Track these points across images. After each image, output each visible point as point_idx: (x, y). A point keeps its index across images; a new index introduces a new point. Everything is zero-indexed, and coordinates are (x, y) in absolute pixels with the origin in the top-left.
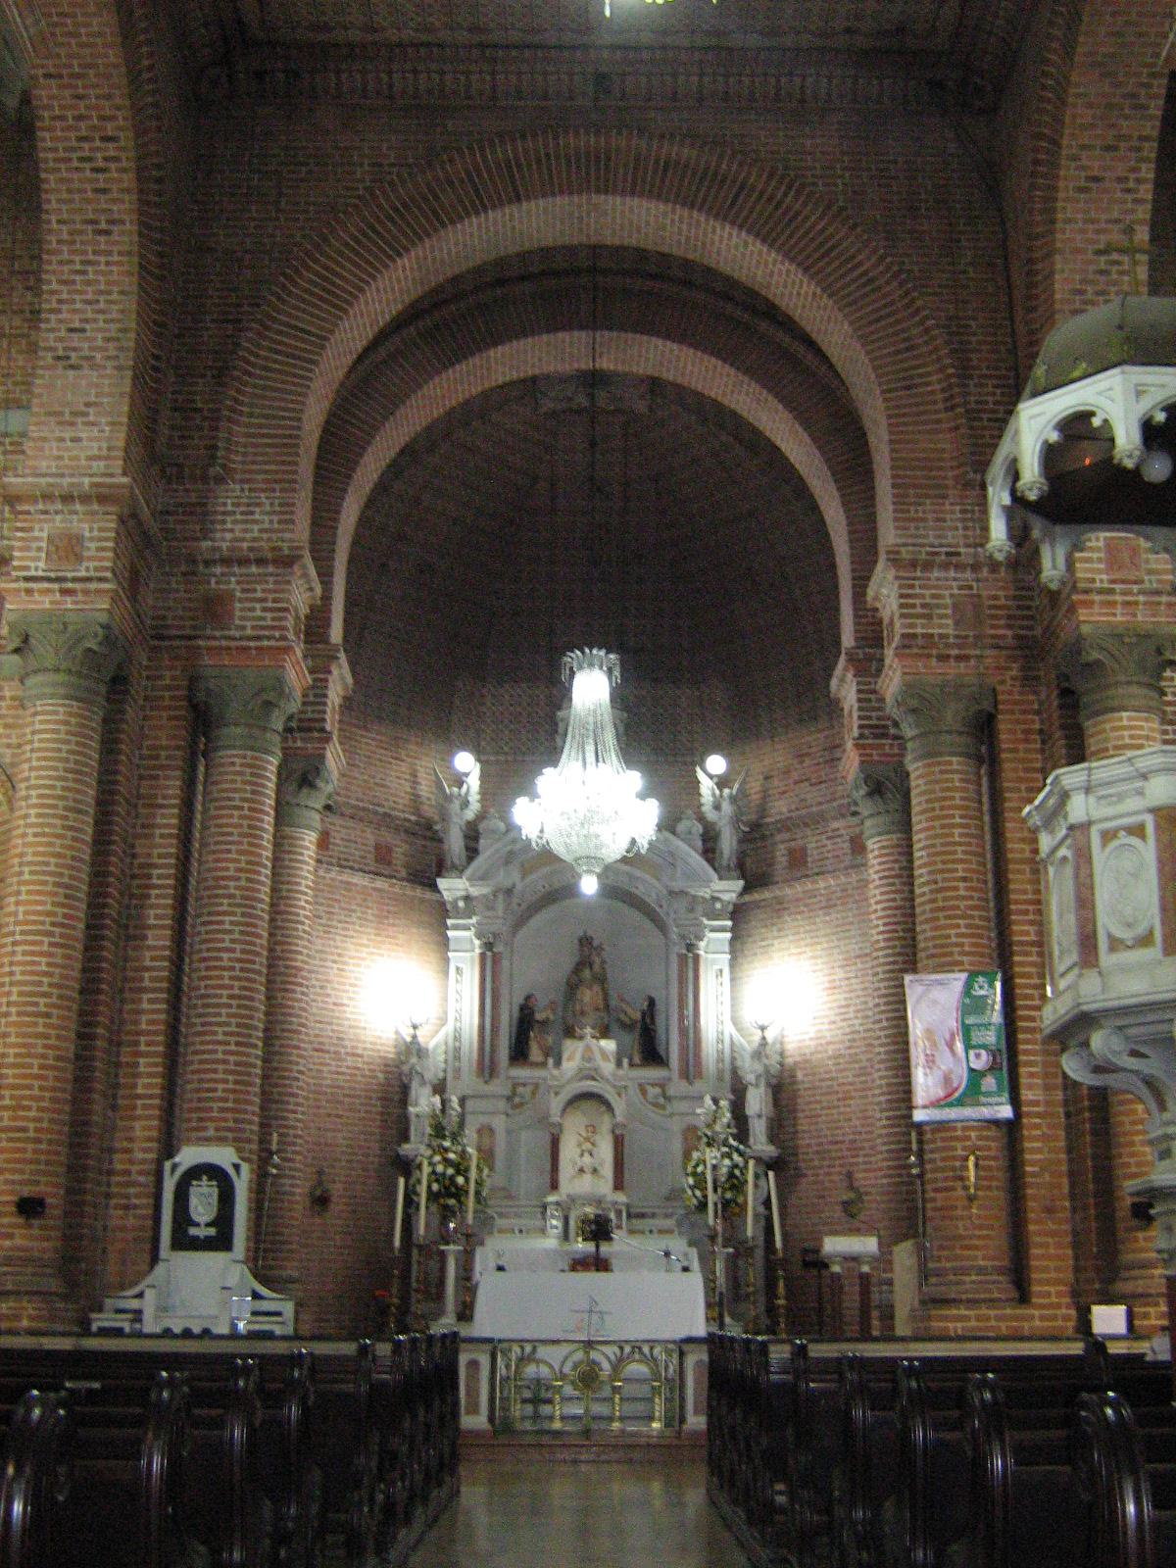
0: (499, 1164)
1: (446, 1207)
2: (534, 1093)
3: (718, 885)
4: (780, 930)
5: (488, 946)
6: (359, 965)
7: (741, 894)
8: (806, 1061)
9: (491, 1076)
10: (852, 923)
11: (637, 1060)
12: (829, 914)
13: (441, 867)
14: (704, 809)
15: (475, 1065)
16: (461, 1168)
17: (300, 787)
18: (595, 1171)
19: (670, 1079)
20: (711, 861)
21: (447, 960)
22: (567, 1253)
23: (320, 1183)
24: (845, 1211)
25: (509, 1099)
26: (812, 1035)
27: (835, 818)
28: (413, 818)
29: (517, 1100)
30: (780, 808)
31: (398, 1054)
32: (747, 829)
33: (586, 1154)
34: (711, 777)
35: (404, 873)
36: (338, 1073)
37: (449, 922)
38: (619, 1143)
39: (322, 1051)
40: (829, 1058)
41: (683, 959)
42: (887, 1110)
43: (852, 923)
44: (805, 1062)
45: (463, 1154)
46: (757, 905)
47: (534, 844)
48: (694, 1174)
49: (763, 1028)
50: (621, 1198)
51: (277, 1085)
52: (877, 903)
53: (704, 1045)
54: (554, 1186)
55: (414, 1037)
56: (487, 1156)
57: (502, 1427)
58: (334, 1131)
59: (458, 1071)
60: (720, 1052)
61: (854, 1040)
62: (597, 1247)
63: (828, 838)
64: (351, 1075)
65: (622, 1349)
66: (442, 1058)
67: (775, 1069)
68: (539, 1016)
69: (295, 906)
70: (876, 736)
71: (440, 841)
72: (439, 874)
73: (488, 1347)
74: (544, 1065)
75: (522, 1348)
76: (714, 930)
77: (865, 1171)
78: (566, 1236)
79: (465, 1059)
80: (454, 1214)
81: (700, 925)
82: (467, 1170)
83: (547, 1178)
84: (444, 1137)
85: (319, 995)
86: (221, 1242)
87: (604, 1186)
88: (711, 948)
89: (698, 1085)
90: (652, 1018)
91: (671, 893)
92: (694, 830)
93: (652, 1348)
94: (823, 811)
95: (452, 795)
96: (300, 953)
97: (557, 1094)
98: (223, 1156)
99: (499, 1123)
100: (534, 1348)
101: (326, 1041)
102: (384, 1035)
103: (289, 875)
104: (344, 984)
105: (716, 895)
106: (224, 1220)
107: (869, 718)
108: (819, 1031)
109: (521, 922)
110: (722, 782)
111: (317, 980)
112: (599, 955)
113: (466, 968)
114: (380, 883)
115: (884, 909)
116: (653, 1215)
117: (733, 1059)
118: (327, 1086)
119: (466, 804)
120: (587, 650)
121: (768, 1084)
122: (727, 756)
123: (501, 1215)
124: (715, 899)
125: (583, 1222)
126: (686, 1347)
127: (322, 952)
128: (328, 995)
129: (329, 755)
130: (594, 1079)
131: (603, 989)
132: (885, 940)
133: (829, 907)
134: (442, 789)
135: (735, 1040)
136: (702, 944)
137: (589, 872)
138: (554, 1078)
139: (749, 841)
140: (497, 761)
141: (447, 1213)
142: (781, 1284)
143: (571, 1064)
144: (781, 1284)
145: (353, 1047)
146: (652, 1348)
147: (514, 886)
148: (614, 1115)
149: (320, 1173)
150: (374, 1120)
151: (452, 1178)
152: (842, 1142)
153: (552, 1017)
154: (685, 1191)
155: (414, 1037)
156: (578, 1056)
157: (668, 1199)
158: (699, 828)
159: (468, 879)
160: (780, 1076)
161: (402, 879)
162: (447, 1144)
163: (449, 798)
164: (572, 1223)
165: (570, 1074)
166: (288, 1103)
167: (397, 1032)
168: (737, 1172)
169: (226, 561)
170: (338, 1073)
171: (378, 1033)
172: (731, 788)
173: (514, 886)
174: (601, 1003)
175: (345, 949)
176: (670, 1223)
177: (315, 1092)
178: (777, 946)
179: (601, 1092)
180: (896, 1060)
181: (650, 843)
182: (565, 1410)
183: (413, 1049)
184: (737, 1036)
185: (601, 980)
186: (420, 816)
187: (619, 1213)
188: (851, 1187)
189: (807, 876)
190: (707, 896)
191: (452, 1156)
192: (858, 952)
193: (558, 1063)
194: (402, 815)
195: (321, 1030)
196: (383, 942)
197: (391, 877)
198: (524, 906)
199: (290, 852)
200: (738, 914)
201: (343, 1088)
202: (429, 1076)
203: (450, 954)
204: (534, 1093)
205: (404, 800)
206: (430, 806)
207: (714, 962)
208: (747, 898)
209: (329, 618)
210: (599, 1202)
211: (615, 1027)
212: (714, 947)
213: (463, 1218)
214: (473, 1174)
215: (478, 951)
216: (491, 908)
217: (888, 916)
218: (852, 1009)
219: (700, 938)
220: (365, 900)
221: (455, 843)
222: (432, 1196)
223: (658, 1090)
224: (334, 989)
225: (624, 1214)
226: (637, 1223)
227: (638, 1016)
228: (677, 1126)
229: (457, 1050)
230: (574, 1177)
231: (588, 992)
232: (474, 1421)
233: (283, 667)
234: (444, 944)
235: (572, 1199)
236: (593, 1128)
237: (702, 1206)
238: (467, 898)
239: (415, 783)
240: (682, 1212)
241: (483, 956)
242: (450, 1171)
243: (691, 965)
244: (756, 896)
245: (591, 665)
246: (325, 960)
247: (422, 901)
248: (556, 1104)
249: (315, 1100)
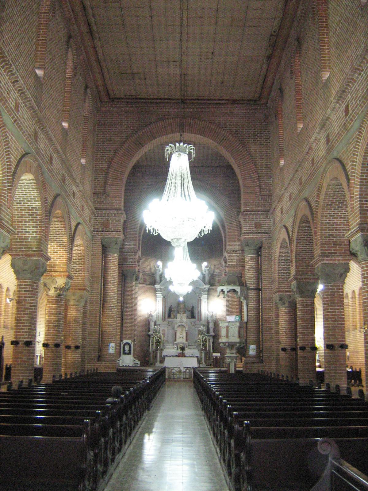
3: (205, 286)
5: (164, 297)
21: (156, 299)
30: (217, 271)
45: (160, 336)
50: (187, 343)
54: (175, 340)
57: (169, 378)
59: (158, 319)
67: (215, 319)
79: (160, 318)
86: (130, 353)
87: (184, 341)
90: (193, 310)
98: (130, 342)
99: (166, 329)
106: (130, 350)
110: (206, 267)
113: (160, 301)
114: (144, 285)
122: (208, 262)
143: (178, 320)
163: (157, 270)
169: (127, 252)
176: (195, 347)
182: (176, 376)
183: (150, 315)
184: (208, 313)
200: (209, 291)
205: (148, 269)
210: (183, 343)
212: (204, 297)
214: (162, 339)
221: (158, 279)
222: (156, 343)
226: (190, 347)
229: (158, 317)
232: (167, 377)
234: (156, 296)
235: (179, 343)
236: (182, 330)
238: (160, 288)
241: (163, 299)
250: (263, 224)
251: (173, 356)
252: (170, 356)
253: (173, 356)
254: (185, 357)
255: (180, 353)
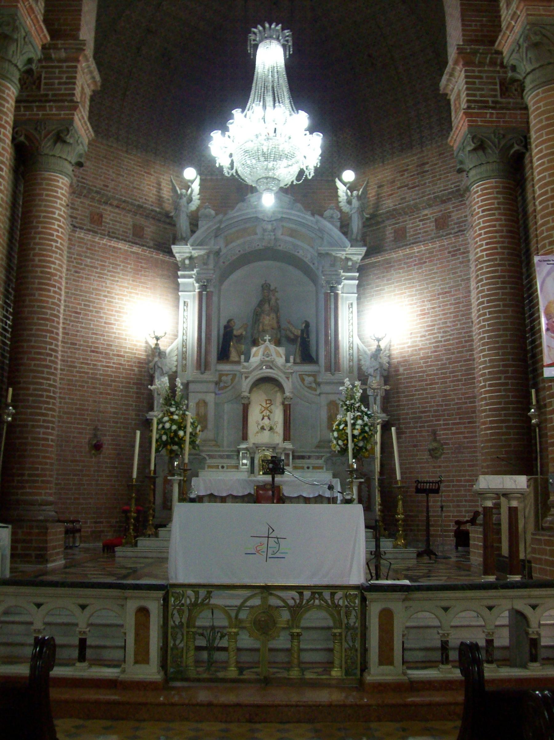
0: (211, 425)
1: (172, 451)
2: (233, 380)
4: (388, 280)
5: (203, 288)
6: (122, 300)
7: (363, 259)
8: (406, 361)
9: (205, 369)
10: (436, 273)
11: (298, 360)
12: (421, 268)
13: (175, 240)
14: (341, 204)
15: (195, 361)
16: (182, 426)
17: (55, 143)
18: (271, 429)
19: (319, 372)
20: (345, 234)
21: (178, 298)
22: (254, 481)
23: (95, 436)
24: (431, 455)
25: (217, 383)
26: (409, 344)
27: (424, 208)
28: (158, 210)
29: (222, 385)
30: (389, 204)
31: (147, 356)
32: (368, 216)
33: (266, 418)
34: (345, 184)
35: (151, 244)
36: (108, 367)
37: (180, 273)
38: (287, 410)
39: (97, 352)
40: (421, 359)
41: (327, 295)
42: (489, 380)
43: (436, 273)
44: (405, 362)
46: (373, 265)
47: (225, 171)
48: (338, 430)
49: (379, 340)
50: (288, 445)
51: (34, 359)
52: (480, 229)
53: (341, 350)
54: (245, 437)
55: (157, 344)
56: (202, 419)
58: (105, 402)
59: (184, 367)
60: (351, 355)
61: (438, 347)
62: (273, 478)
63: (420, 221)
64: (116, 368)
65: (301, 594)
66: (175, 358)
68: (235, 333)
69: (50, 229)
70: (479, 108)
71: (174, 225)
72: (174, 244)
73: (160, 594)
74: (238, 362)
75: (197, 594)
76: (347, 278)
77: (445, 429)
78: (252, 471)
79: (189, 358)
80: (177, 455)
81: (338, 275)
82: (185, 427)
83: (241, 434)
84: (171, 405)
85: (95, 316)
87: (278, 438)
88: (345, 290)
89: (338, 375)
91: (320, 255)
92: (334, 216)
93: (333, 595)
94: (416, 203)
95: (181, 194)
96: (54, 263)
97: (246, 378)
99: (210, 398)
100: (209, 593)
101: (101, 346)
102: (138, 344)
103: (46, 206)
104: (112, 311)
105: (348, 256)
107: (475, 95)
108: (415, 342)
109: (224, 276)
110: (351, 187)
111: (95, 307)
112: (274, 295)
114: (135, 249)
115: (486, 233)
116: (309, 457)
117: (359, 360)
118: (101, 375)
119: (190, 200)
120: (267, 25)
121: (382, 375)
123: (211, 457)
124: (347, 259)
125: (263, 461)
126: (368, 595)
127: (96, 289)
128: (101, 317)
129: (76, 118)
130: (271, 368)
131: (277, 317)
132: (487, 255)
133: (421, 263)
134: (176, 191)
135: (360, 348)
136: (340, 287)
137: (268, 189)
138: (244, 367)
139: (369, 226)
140: (212, 179)
141: (173, 455)
142: (400, 503)
144: (400, 503)
145: (118, 351)
146: (333, 595)
147: (220, 250)
148: (283, 392)
149: (96, 429)
150: (132, 397)
151: (176, 432)
152: (430, 411)
153: (244, 333)
154: (331, 441)
155: (157, 344)
156: (261, 353)
157: (318, 447)
158: (338, 214)
159: (192, 245)
160: (388, 370)
161: (149, 247)
162: (173, 409)
163: (180, 196)
164: (256, 462)
165: (255, 365)
166: (43, 372)
167: (147, 342)
168: (367, 428)
170: (108, 367)
171: (135, 343)
172: (358, 190)
173: (220, 250)
174: (275, 325)
175: (113, 289)
176: (321, 462)
177: (92, 378)
178: (386, 290)
179: (275, 376)
180: (497, 342)
181: (316, 169)
184: (361, 346)
185: (276, 310)
186: (162, 209)
187: (287, 455)
188: (435, 440)
189: (407, 245)
190: (343, 257)
191: (175, 417)
192: (440, 291)
193: (247, 359)
194: (151, 208)
195: (96, 338)
196: (139, 286)
197: (143, 246)
198: (227, 263)
199: (48, 190)
201: (111, 376)
202: (165, 369)
203: (180, 293)
204: (233, 380)
206: (169, 204)
207: (347, 298)
208: (367, 261)
209: (80, 25)
211: (283, 340)
213: (183, 459)
214: (189, 429)
215: (197, 290)
216: (205, 264)
217: (490, 238)
218: (436, 327)
219: (339, 284)
220: (127, 259)
221: (183, 224)
222: (161, 444)
223: (311, 379)
224: (105, 313)
225: (291, 457)
227: (299, 333)
228: (323, 401)
229: (184, 358)
230: (257, 433)
231: (267, 318)
233: (16, 6)
234: (177, 288)
235: (257, 447)
236: (270, 402)
237: (344, 451)
238: (191, 258)
239: (159, 189)
240: (328, 455)
241: (200, 294)
242: (174, 427)
243: (333, 300)
244: (373, 260)
245: (270, 37)
246: (100, 295)
247: (163, 261)
248: (246, 384)
249: (92, 383)
250: (448, 481)
251: (235, 499)
252: (223, 500)
253: (235, 499)
254: (281, 499)
255: (260, 487)
